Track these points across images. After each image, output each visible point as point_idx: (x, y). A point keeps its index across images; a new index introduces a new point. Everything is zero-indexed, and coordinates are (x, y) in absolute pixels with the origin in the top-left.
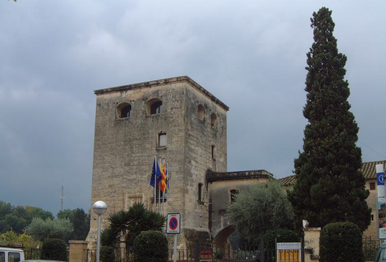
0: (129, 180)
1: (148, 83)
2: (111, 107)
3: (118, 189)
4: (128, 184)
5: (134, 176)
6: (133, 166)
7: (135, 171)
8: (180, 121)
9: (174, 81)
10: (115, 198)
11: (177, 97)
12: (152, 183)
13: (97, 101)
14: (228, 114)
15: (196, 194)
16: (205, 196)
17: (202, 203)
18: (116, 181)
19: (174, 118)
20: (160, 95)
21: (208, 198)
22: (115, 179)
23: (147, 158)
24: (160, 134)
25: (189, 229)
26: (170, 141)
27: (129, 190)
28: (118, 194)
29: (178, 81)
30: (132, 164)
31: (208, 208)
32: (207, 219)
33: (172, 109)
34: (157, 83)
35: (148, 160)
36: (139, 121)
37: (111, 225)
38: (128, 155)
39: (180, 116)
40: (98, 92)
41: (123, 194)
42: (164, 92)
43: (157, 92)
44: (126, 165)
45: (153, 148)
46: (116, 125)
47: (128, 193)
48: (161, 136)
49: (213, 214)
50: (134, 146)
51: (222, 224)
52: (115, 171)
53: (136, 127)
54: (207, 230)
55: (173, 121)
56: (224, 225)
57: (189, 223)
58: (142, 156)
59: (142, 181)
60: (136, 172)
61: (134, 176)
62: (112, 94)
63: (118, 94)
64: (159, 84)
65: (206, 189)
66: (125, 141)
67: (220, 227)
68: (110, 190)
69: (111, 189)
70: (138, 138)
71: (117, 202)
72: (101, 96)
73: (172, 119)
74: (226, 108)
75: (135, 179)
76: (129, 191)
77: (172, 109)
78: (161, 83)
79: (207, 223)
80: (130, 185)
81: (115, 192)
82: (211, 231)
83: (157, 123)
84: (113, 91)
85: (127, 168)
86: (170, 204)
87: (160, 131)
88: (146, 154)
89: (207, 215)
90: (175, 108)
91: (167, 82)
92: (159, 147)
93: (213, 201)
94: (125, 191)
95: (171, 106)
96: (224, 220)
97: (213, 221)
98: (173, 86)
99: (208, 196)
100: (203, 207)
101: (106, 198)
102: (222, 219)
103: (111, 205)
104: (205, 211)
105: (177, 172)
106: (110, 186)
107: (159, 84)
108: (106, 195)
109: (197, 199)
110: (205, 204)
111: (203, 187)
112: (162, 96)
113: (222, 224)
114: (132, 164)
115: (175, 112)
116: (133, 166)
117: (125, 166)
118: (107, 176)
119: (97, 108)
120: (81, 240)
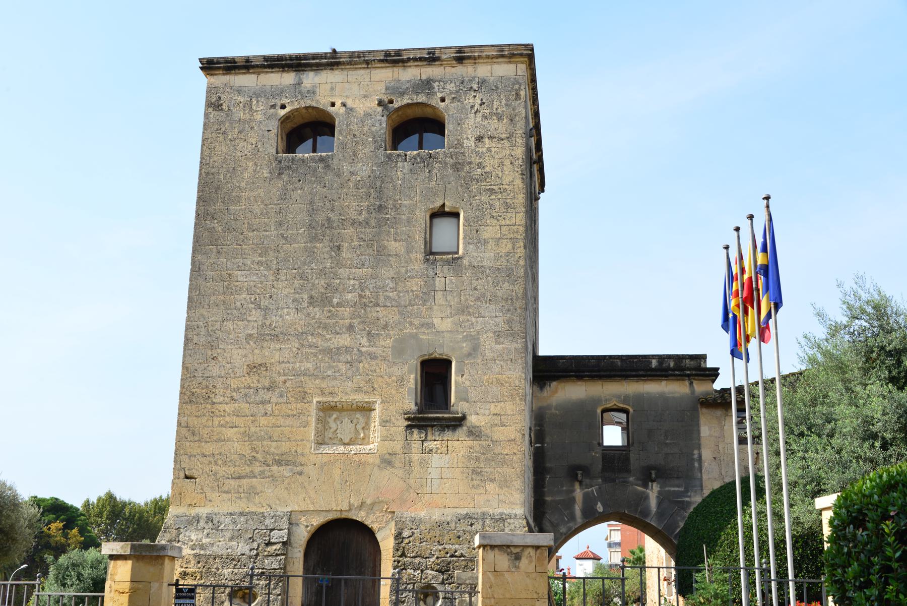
0: (328, 351)
1: (398, 52)
2: (259, 117)
5: (345, 340)
6: (339, 305)
7: (347, 322)
8: (507, 180)
9: (488, 57)
10: (269, 407)
12: (725, 326)
13: (209, 92)
18: (272, 353)
19: (487, 169)
22: (275, 345)
24: (439, 214)
26: (476, 239)
29: (503, 56)
30: (335, 301)
33: (480, 139)
34: (431, 57)
36: (363, 170)
37: (544, 488)
38: (322, 272)
39: (507, 162)
40: (209, 66)
41: (303, 396)
43: (427, 85)
44: (312, 301)
47: (323, 393)
48: (437, 221)
52: (274, 319)
59: (373, 357)
60: (350, 328)
61: (345, 340)
62: (262, 76)
63: (288, 78)
64: (437, 59)
66: (311, 227)
68: (253, 381)
70: (361, 218)
71: (281, 421)
72: (221, 80)
75: (348, 350)
76: (323, 385)
77: (480, 139)
78: (444, 57)
80: (330, 367)
82: (477, 532)
84: (271, 67)
85: (316, 312)
87: (438, 204)
88: (386, 273)
91: (462, 56)
92: (432, 253)
93: (547, 439)
94: (310, 385)
95: (477, 133)
96: (586, 497)
98: (483, 70)
102: (579, 493)
105: (498, 335)
106: (253, 368)
107: (437, 59)
114: (335, 301)
115: (489, 150)
116: (339, 305)
118: (242, 336)
119: (206, 115)
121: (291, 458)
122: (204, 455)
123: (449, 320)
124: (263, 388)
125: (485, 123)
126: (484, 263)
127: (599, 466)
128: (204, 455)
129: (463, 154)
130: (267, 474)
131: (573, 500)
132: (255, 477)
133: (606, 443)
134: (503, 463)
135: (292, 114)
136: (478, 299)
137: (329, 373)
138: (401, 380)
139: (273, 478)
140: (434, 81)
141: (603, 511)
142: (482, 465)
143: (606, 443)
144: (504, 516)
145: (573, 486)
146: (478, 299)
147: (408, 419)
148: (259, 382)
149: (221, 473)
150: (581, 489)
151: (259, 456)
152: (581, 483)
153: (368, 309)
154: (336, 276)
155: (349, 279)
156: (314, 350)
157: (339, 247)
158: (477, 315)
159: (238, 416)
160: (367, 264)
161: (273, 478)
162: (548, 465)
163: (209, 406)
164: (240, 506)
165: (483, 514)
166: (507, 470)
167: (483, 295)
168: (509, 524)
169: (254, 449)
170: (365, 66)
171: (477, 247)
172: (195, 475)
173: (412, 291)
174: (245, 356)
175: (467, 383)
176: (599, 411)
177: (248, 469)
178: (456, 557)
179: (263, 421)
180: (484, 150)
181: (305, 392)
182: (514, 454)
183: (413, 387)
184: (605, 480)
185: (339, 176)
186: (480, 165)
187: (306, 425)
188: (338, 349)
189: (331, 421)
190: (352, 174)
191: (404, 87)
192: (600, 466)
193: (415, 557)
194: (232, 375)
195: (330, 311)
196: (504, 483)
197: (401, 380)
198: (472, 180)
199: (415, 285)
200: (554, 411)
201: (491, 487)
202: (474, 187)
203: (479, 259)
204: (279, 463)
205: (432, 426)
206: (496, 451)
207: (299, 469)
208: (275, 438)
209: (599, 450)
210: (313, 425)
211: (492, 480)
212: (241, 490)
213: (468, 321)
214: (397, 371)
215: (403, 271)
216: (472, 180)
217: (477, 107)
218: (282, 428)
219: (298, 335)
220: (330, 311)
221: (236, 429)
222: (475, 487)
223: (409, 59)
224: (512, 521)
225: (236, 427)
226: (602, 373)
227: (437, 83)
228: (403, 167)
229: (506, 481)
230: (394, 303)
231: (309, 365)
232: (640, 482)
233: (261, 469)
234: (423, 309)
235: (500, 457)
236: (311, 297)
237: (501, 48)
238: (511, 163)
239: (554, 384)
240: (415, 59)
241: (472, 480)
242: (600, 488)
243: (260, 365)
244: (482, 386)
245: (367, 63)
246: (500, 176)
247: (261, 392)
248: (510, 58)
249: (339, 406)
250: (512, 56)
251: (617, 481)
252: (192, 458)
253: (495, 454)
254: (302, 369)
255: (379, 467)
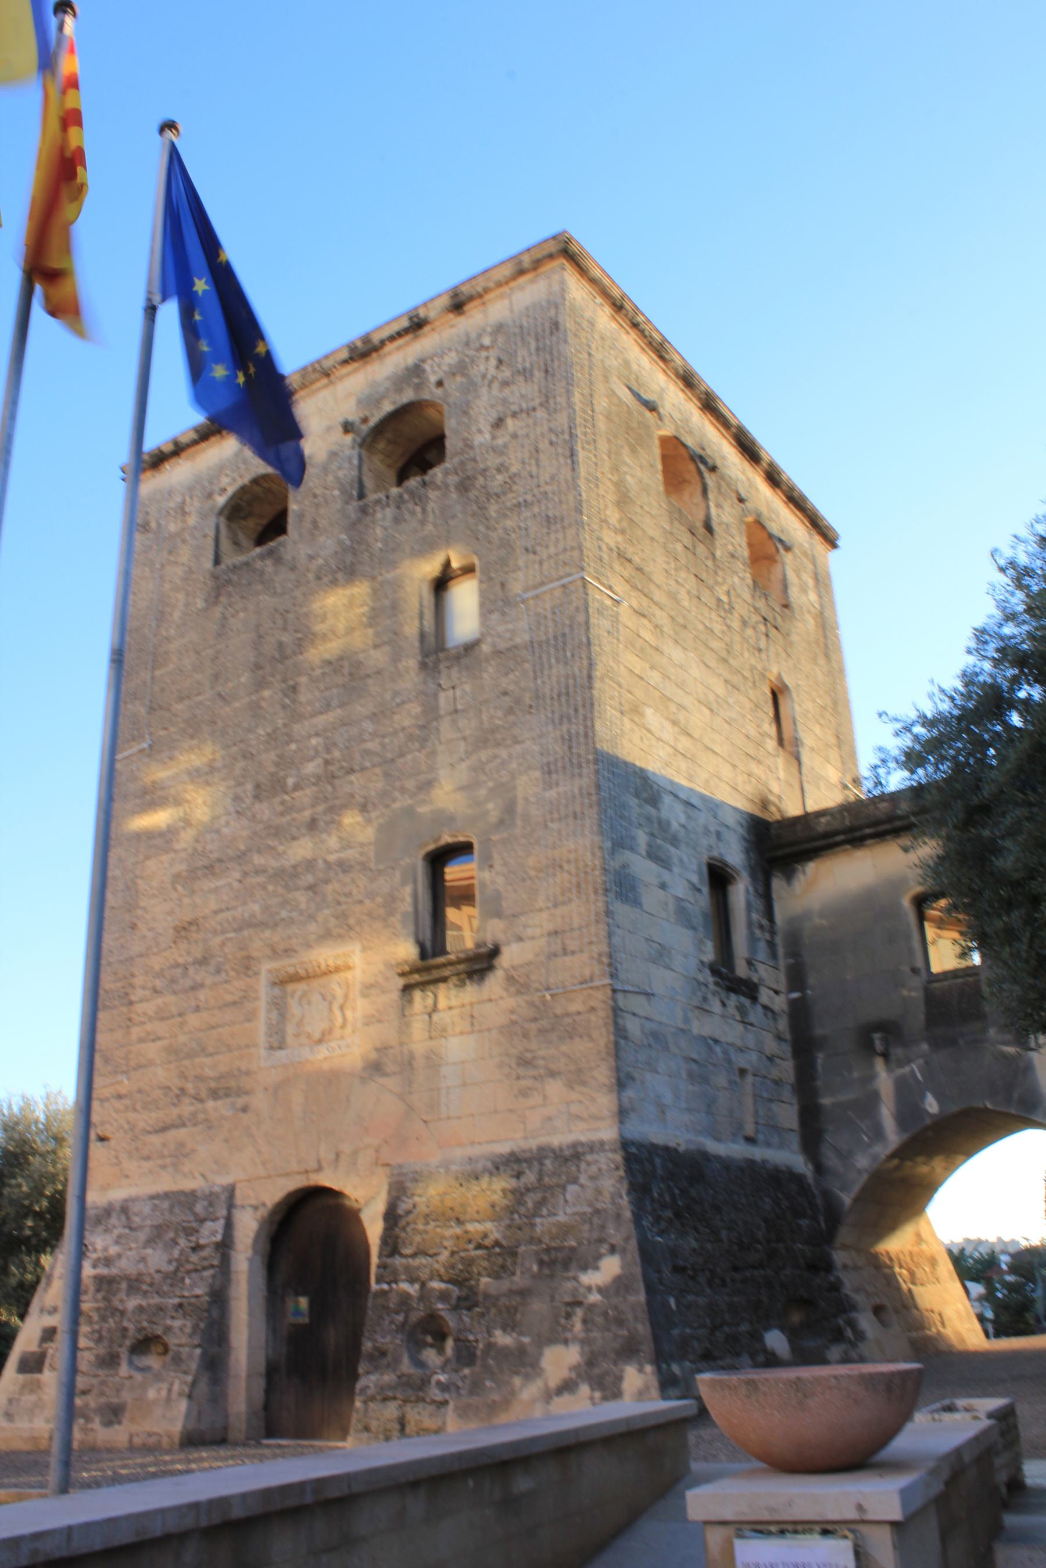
0: (279, 875)
1: (366, 339)
3: (218, 940)
4: (274, 901)
6: (297, 787)
7: (307, 814)
9: (499, 284)
10: (202, 995)
11: (524, 357)
14: (835, 561)
15: (698, 921)
16: (762, 946)
17: (748, 989)
20: (433, 379)
21: (782, 963)
23: (369, 726)
25: (667, 1149)
27: (276, 937)
28: (218, 971)
30: (290, 782)
31: (783, 1024)
32: (787, 1094)
33: (499, 423)
35: (374, 735)
38: (272, 737)
39: (544, 445)
42: (451, 358)
43: (416, 370)
45: (401, 665)
46: (217, 596)
49: (820, 1058)
50: (303, 680)
51: (887, 1114)
53: (311, 576)
54: (792, 1158)
55: (508, 487)
56: (902, 1120)
57: (662, 1109)
58: (344, 724)
65: (758, 904)
67: (878, 1134)
69: (183, 946)
73: (500, 478)
74: (830, 539)
75: (310, 865)
77: (499, 423)
78: (432, 315)
79: (788, 1115)
80: (285, 902)
81: (203, 962)
82: (819, 1168)
83: (423, 522)
85: (264, 810)
86: (516, 983)
88: (361, 708)
89: (786, 1069)
90: (514, 415)
93: (812, 980)
95: (494, 415)
97: (826, 1101)
99: (781, 951)
100: (756, 1015)
101: (159, 1001)
102: (884, 1080)
103: (182, 1039)
104: (771, 1045)
108: (159, 983)
109: (709, 954)
110: (765, 996)
111: (740, 893)
112: (440, 384)
113: (887, 1114)
114: (290, 782)
117: (257, 797)
120: (889, 1361)
121: (232, 1083)
122: (120, 1097)
123: (464, 766)
124: (194, 963)
125: (507, 391)
126: (518, 640)
127: (918, 1018)
128: (120, 1097)
129: (474, 460)
130: (201, 1116)
131: (874, 1098)
132: (184, 1125)
133: (936, 968)
134: (571, 1034)
135: (241, 499)
136: (510, 711)
137: (284, 914)
138: (391, 900)
139: (209, 1124)
140: (423, 361)
141: (941, 1111)
142: (533, 1046)
143: (936, 968)
144: (580, 1150)
145: (871, 1066)
146: (510, 711)
147: (403, 974)
148: (188, 953)
149: (142, 1125)
150: (889, 1070)
151: (190, 1087)
152: (885, 1056)
153: (337, 782)
154: (291, 739)
155: (310, 736)
156: (261, 879)
157: (294, 689)
158: (509, 742)
159: (162, 1019)
160: (335, 702)
161: (209, 1124)
162: (819, 1032)
163: (124, 1009)
164: (167, 1183)
165: (541, 1149)
166: (580, 1047)
167: (518, 701)
168: (589, 1164)
169: (183, 1076)
170: (325, 381)
171: (504, 614)
172: (108, 1134)
173: (403, 729)
174: (171, 913)
175: (500, 880)
176: (906, 903)
177: (175, 1111)
178: (486, 1248)
179: (193, 1020)
180: (507, 438)
181: (249, 957)
182: (593, 1009)
183: (410, 909)
184: (936, 1044)
185: (293, 569)
186: (501, 469)
187: (251, 1017)
188: (294, 867)
189: (293, 1005)
190: (311, 558)
191: (382, 389)
192: (922, 1017)
193: (415, 1255)
194: (155, 950)
195: (283, 803)
196: (577, 1078)
197: (391, 900)
198: (489, 496)
199: (409, 715)
200: (817, 921)
201: (555, 1088)
202: (493, 509)
203: (508, 635)
204: (215, 1094)
205: (444, 980)
206: (559, 1011)
207: (241, 1102)
208: (211, 1050)
209: (917, 982)
210: (262, 1014)
211: (553, 1074)
212: (166, 1152)
213: (495, 757)
214: (383, 885)
215: (388, 696)
216: (489, 496)
217: (492, 371)
218: (221, 1030)
219: (241, 857)
220: (283, 803)
221: (159, 1043)
222: (524, 1093)
223: (383, 343)
224: (595, 1156)
225: (159, 1039)
226: (881, 828)
227: (430, 362)
228: (384, 519)
229: (580, 1071)
230: (377, 760)
231: (256, 908)
232: (1009, 1037)
233: (192, 1108)
234: (421, 756)
235: (568, 1020)
236: (258, 786)
237: (515, 259)
238: (551, 443)
239: (811, 867)
240: (392, 338)
241: (518, 1078)
242: (927, 1063)
243: (190, 923)
244: (524, 880)
245: (327, 374)
246: (534, 473)
247: (191, 971)
248: (535, 269)
249: (302, 972)
250: (537, 264)
251: (961, 1042)
252: (106, 1105)
253: (556, 1016)
254: (246, 915)
255: (362, 1078)
